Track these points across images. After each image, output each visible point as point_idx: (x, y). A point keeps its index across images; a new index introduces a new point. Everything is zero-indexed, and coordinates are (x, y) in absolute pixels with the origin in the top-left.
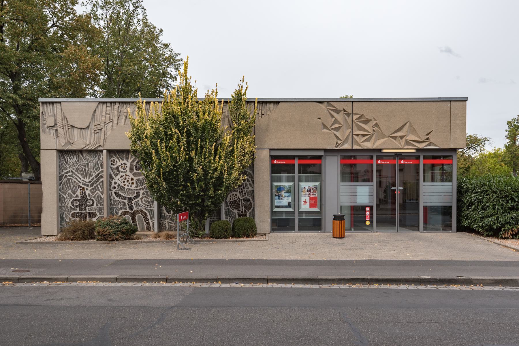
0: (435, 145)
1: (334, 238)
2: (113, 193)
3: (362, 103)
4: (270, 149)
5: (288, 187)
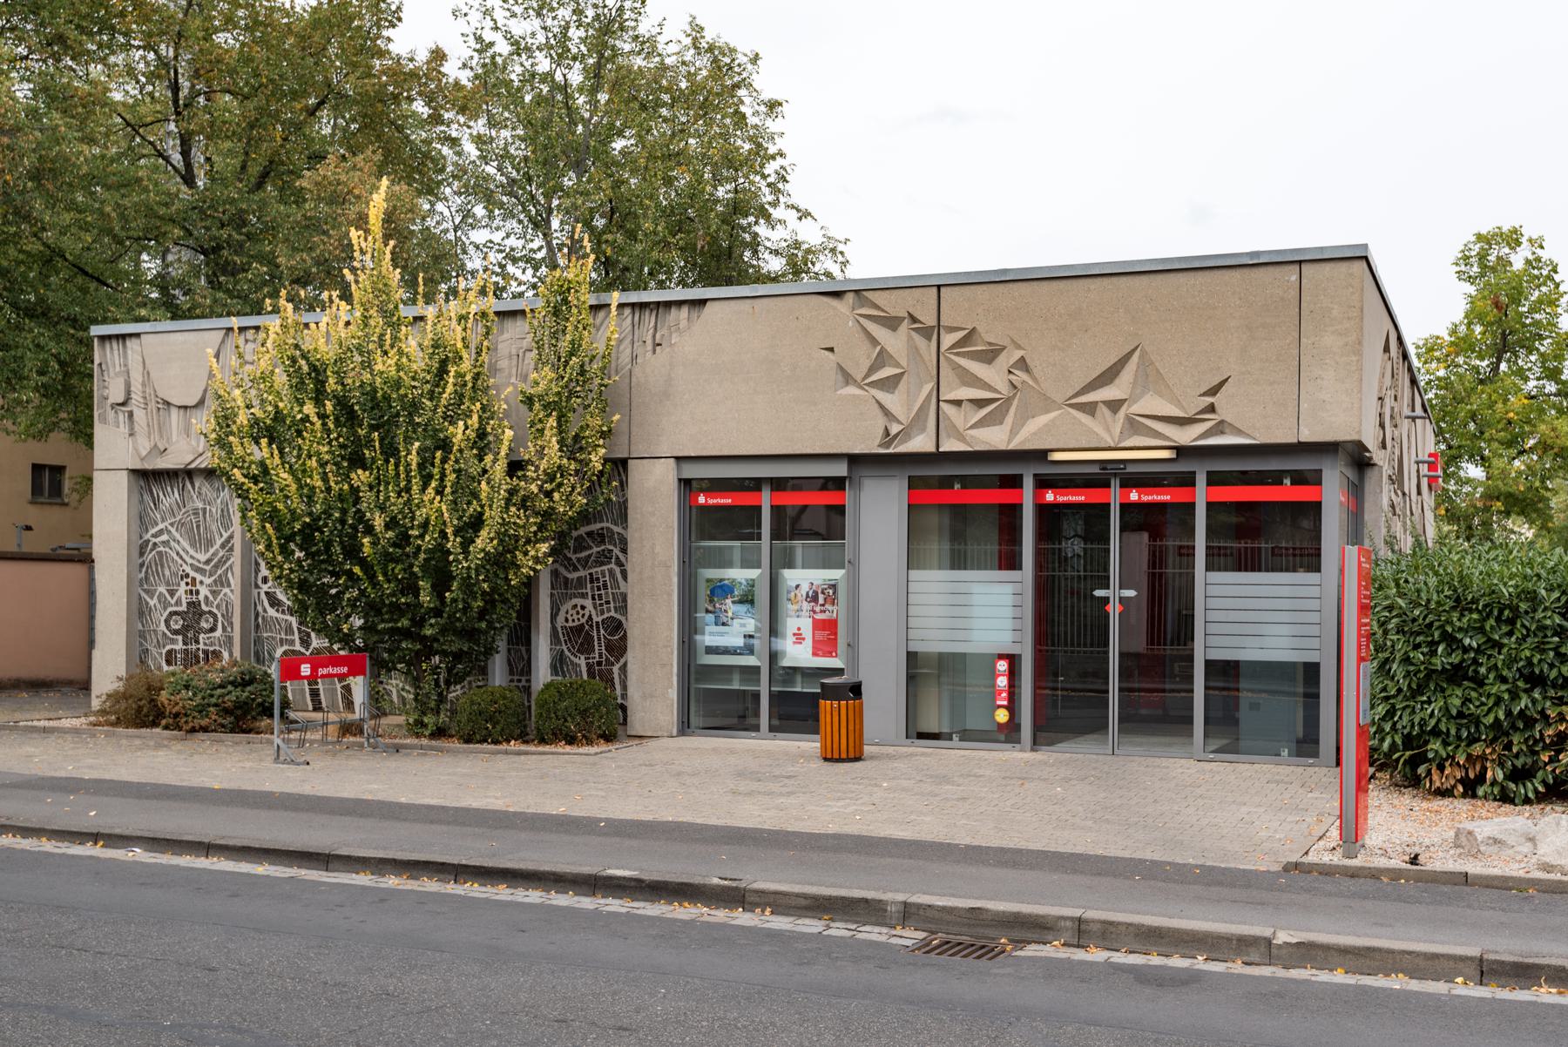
0: (1239, 432)
1: (826, 759)
2: (263, 596)
3: (972, 287)
4: (678, 459)
5: (744, 582)
